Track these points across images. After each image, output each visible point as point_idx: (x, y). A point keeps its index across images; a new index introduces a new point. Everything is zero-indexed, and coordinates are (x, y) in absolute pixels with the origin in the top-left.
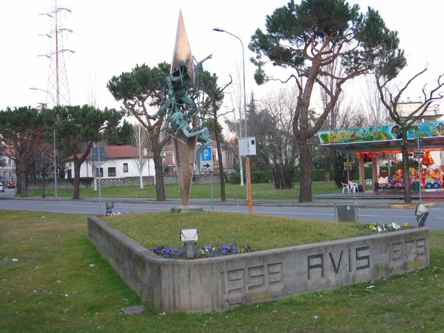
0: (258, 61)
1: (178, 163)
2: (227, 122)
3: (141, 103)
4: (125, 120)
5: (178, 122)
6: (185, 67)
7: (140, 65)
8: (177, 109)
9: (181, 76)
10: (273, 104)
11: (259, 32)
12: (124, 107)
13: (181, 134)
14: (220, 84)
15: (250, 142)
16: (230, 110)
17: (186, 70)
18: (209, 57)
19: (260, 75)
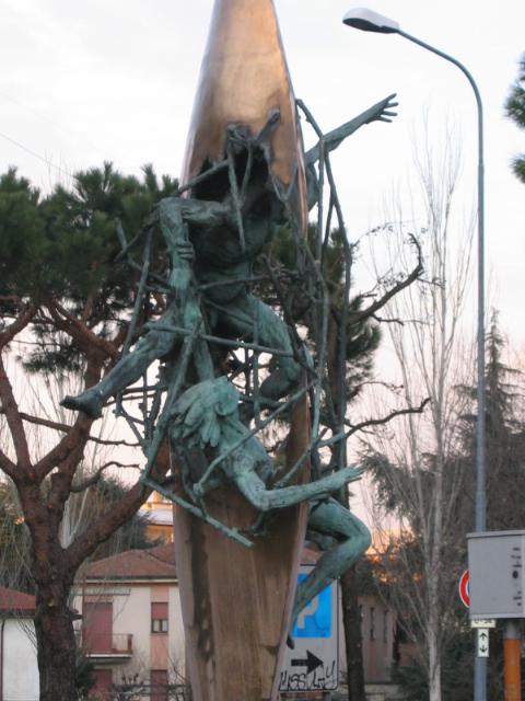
1: (200, 644)
5: (210, 432)
6: (258, 152)
9: (236, 202)
13: (225, 492)
14: (363, 281)
16: (399, 401)
17: (261, 169)
18: (378, 113)
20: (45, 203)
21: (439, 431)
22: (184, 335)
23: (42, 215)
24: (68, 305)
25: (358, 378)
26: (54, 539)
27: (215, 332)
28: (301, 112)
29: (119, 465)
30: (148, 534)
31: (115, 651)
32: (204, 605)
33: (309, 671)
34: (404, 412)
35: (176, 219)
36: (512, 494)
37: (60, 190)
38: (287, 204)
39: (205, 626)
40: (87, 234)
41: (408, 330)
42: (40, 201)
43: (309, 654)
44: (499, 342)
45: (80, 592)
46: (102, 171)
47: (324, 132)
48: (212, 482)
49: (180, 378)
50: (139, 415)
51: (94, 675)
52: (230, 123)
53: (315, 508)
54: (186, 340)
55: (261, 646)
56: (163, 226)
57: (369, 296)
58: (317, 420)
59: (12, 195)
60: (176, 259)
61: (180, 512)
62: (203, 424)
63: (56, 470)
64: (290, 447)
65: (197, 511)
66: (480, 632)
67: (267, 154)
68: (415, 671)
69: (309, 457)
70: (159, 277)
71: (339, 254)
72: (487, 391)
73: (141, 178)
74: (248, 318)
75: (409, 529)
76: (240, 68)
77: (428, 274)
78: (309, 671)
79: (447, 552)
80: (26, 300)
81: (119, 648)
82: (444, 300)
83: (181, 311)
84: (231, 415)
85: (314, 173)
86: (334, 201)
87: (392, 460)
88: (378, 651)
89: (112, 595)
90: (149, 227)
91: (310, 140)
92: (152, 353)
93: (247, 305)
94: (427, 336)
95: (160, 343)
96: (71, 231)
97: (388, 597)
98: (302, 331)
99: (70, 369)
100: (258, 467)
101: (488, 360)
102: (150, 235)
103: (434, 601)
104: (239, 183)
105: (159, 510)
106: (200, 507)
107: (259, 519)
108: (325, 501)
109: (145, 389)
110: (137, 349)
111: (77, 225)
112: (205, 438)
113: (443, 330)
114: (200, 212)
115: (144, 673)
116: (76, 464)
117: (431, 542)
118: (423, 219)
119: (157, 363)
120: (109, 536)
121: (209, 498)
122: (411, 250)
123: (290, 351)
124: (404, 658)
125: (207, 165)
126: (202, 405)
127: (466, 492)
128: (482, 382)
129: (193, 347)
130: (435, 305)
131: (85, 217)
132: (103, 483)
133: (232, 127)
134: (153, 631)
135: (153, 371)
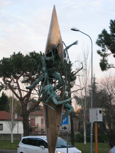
0: (103, 53)
1: (47, 125)
2: (76, 97)
3: (15, 80)
4: (3, 92)
5: (49, 93)
6: (56, 49)
7: (16, 53)
8: (48, 82)
9: (53, 57)
10: (110, 86)
11: (104, 32)
12: (3, 82)
13: (51, 101)
14: (73, 69)
15: (99, 112)
16: (79, 88)
17: (57, 52)
18: (75, 43)
19: (104, 63)
20: (25, 57)
21: (86, 92)
22: (45, 78)
23: (24, 59)
24: (28, 73)
25: (73, 84)
26: (26, 109)
27: (50, 77)
28: (63, 43)
29: (36, 98)
30: (41, 108)
31: (36, 126)
32: (48, 119)
33: (65, 129)
34: (80, 89)
35: (44, 60)
36: (97, 102)
37: (27, 55)
38: (61, 57)
39: (48, 122)
40: (31, 62)
41: (81, 77)
42: (24, 57)
43: (65, 127)
44: (95, 79)
45: (30, 117)
46: (34, 52)
47: (67, 46)
48: (49, 100)
49: (44, 84)
50: (38, 90)
51: (32, 130)
52: (52, 45)
53: (65, 104)
54: (45, 78)
55: (57, 126)
56: (42, 61)
57: (75, 72)
58: (65, 90)
59: (20, 56)
60: (43, 66)
61: (44, 105)
62: (47, 91)
63: (26, 98)
64: (61, 95)
65: (47, 105)
66: (92, 123)
67: (58, 50)
68: (82, 129)
69: (64, 96)
70: (41, 69)
71: (70, 65)
72: (93, 86)
73: (40, 53)
74: (55, 75)
75: (81, 108)
76: (54, 36)
77: (84, 68)
78: (65, 129)
79: (87, 111)
80: (22, 72)
81: (36, 126)
82: (86, 72)
83: (44, 74)
84: (52, 90)
85: (65, 53)
86: (68, 57)
87: (78, 97)
88: (76, 126)
89: (35, 117)
90: (39, 61)
91: (64, 48)
92: (40, 80)
93: (55, 73)
94: (84, 78)
95: (41, 79)
96: (29, 61)
97: (78, 118)
98: (63, 77)
99: (29, 83)
100: (56, 98)
101: (93, 81)
102: (39, 62)
103: (85, 119)
104: (53, 54)
105: (41, 104)
106: (47, 104)
107: (56, 106)
108: (67, 103)
109: (39, 86)
110: (38, 80)
111: (30, 60)
112: (48, 94)
113: (86, 77)
114: (47, 58)
115: (40, 129)
116: (29, 97)
117: (84, 110)
118: (83, 60)
119: (40, 82)
120: (34, 108)
121: (48, 103)
122: (81, 64)
123: (61, 80)
124: (80, 127)
125: (48, 51)
126: (47, 88)
127: (90, 102)
128: (92, 85)
129: (46, 79)
130: (85, 73)
131: (31, 59)
132: (34, 100)
133: (52, 45)
134: (41, 123)
135: (40, 83)
